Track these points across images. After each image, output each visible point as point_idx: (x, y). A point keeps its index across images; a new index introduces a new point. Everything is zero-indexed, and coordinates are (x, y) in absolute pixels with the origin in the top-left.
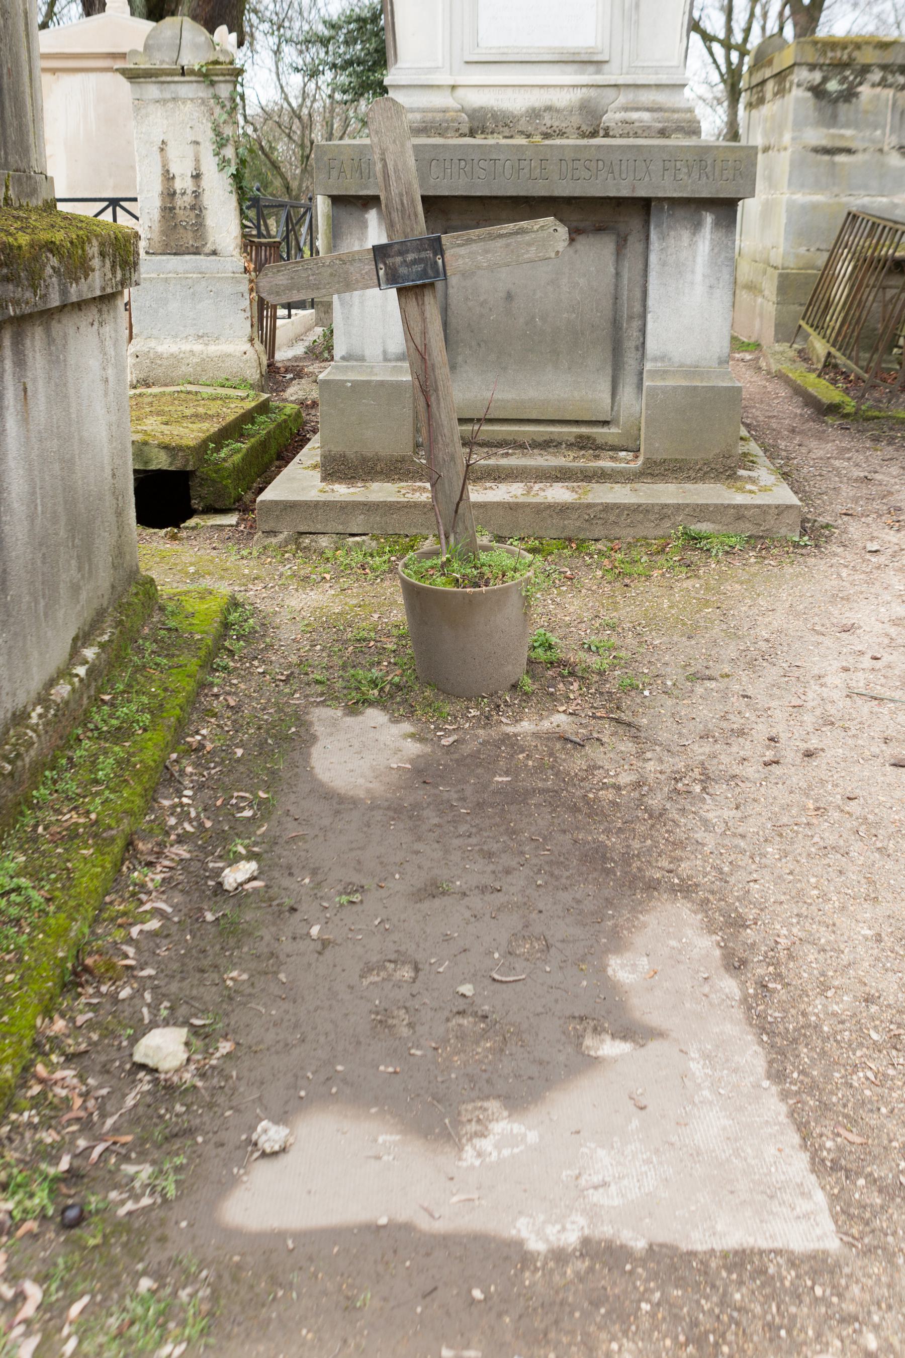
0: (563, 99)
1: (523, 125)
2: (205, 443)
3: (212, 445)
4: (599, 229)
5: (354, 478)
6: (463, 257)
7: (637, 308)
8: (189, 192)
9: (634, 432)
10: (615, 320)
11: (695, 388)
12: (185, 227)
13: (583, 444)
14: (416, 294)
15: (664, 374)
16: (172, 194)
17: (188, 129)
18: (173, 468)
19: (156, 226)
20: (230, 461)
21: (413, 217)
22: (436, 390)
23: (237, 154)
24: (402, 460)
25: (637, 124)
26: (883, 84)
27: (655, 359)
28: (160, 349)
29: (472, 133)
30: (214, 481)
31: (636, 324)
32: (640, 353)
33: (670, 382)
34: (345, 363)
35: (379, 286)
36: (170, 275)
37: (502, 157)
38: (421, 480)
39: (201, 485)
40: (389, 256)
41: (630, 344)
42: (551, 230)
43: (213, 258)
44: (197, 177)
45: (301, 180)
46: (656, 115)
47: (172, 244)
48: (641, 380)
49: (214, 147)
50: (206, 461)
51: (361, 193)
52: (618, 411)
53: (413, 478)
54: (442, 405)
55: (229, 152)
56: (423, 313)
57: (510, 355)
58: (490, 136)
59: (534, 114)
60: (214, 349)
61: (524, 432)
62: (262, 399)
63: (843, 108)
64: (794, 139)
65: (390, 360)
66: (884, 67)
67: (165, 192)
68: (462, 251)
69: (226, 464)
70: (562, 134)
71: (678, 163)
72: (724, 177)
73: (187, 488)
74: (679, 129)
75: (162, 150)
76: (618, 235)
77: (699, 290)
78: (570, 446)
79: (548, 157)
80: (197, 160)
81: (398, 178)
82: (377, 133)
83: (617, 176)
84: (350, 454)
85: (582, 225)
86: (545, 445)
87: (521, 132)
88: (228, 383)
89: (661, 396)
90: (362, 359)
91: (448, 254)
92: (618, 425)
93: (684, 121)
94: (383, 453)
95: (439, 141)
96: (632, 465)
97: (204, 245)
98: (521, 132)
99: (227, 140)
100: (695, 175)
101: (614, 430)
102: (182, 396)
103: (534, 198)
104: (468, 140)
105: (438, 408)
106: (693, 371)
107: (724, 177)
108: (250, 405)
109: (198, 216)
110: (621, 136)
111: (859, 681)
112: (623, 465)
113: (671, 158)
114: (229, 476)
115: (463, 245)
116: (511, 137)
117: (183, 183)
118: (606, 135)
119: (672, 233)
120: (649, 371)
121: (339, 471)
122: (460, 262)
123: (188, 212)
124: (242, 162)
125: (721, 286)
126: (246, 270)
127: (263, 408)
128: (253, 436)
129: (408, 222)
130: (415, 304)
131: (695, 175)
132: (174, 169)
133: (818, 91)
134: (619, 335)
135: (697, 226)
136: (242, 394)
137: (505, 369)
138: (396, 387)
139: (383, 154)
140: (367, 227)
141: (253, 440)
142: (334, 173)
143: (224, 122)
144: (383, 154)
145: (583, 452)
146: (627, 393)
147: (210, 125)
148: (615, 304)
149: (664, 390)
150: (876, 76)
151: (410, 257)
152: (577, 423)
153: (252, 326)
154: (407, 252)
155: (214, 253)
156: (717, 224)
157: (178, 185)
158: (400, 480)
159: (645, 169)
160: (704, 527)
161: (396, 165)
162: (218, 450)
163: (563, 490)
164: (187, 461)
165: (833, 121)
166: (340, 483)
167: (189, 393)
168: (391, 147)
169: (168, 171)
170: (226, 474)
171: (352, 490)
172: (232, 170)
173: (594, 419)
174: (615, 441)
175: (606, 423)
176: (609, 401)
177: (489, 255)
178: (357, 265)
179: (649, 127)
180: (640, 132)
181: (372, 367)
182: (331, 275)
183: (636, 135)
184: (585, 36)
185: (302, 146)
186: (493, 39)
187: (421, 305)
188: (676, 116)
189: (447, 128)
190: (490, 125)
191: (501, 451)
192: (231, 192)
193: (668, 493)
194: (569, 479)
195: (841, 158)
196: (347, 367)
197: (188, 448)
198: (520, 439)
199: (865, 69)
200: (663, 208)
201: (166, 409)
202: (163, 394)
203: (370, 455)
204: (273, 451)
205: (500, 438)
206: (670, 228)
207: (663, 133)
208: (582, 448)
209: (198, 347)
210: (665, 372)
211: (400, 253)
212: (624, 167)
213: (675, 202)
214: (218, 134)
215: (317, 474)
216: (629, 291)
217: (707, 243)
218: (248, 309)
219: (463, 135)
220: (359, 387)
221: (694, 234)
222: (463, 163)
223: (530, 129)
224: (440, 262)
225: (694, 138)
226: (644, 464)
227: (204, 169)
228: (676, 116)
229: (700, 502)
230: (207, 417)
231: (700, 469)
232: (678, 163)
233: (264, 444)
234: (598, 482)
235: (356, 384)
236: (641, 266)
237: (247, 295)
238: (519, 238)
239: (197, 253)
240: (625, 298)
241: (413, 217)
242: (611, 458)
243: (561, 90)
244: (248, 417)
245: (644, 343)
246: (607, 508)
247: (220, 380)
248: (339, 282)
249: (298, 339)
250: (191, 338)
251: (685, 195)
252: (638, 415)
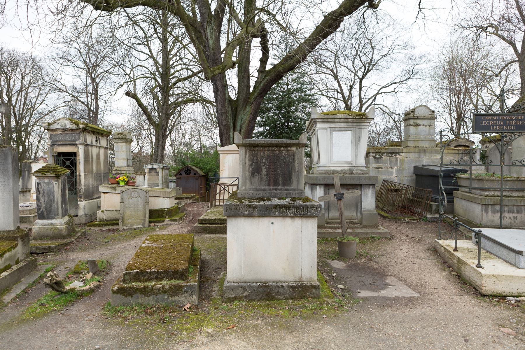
0: (346, 168)
26: (387, 156)
59: (342, 171)
63: (380, 160)
66: (387, 153)
77: (370, 198)
95: (327, 175)
106: (370, 211)
111: (405, 255)
133: (375, 157)
135: (369, 188)
150: (386, 154)
160: (374, 236)
165: (378, 163)
184: (349, 159)
186: (335, 159)
193: (367, 230)
195: (380, 169)
199: (383, 153)
207: (363, 174)
213: (366, 184)
226: (335, 268)
229: (317, 242)
243: (346, 167)
246: (358, 233)
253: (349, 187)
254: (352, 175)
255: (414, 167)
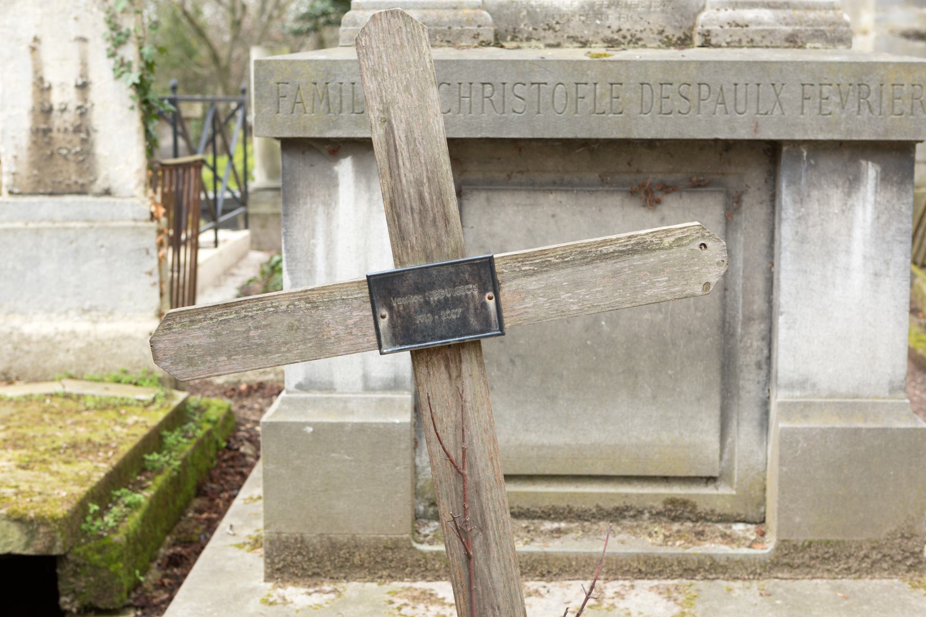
1: (575, 27)
2: (82, 506)
3: (94, 507)
4: (698, 185)
5: (318, 574)
6: (534, 294)
7: (759, 305)
8: (72, 107)
9: (756, 493)
10: (724, 321)
11: (857, 431)
12: (65, 157)
13: (676, 511)
14: (447, 360)
15: (804, 409)
16: (47, 112)
17: (71, 21)
18: (30, 552)
19: (24, 156)
20: (122, 531)
21: (440, 224)
22: (483, 528)
23: (141, 56)
24: (395, 546)
25: (753, 27)
27: (791, 386)
28: (27, 329)
29: (498, 41)
30: (96, 567)
31: (758, 328)
32: (763, 373)
33: (816, 423)
34: (303, 395)
35: (380, 347)
36: (44, 225)
37: (550, 79)
38: (424, 578)
39: (75, 574)
40: (398, 295)
41: (748, 358)
42: (696, 245)
43: (106, 199)
44: (83, 87)
45: (232, 49)
46: (781, 14)
47: (48, 180)
48: (766, 414)
49: (109, 45)
50: (85, 533)
51: (328, 135)
52: (731, 460)
53: (412, 576)
54: (494, 553)
55: (130, 52)
56: (459, 395)
57: (561, 377)
58: (524, 44)
60: (106, 329)
61: (584, 495)
62: (175, 403)
64: (877, 21)
65: (373, 390)
67: (38, 108)
68: (532, 283)
69: (116, 538)
70: (635, 41)
71: (825, 89)
72: (897, 110)
73: (54, 578)
74: (818, 35)
75: (33, 49)
76: (728, 194)
77: (858, 279)
78: (657, 516)
79: (622, 79)
80: (84, 64)
81: (414, 153)
82: (375, 73)
83: (730, 108)
84: (312, 537)
85: (670, 179)
86: (618, 514)
87: (573, 39)
88: (125, 378)
89: (803, 444)
90: (329, 387)
91: (506, 291)
92: (730, 482)
93: (825, 22)
94: (364, 536)
96: (757, 551)
97: (93, 182)
98: (573, 39)
99: (127, 36)
100: (852, 107)
101: (723, 490)
102: (57, 403)
103: (597, 140)
104: (492, 53)
105: (487, 559)
106: (850, 405)
107: (897, 110)
108: (157, 416)
109: (84, 141)
110: (729, 45)
112: (744, 551)
113: (814, 81)
114: (120, 557)
115: (533, 273)
116: (558, 45)
117: (63, 96)
118: (707, 44)
119: (815, 194)
120: (782, 405)
121: (294, 564)
122: (529, 303)
123: (70, 137)
124: (149, 66)
125: (891, 273)
126: (153, 217)
127: (178, 418)
128: (160, 471)
129: (431, 231)
130: (444, 376)
131: (852, 107)
132: (50, 77)
134: (732, 346)
135: (854, 182)
136: (144, 394)
137: (553, 399)
138: (384, 433)
139: (386, 110)
140: (336, 185)
141: (160, 479)
142: (286, 104)
143: (124, 11)
144: (386, 110)
145: (676, 526)
146: (744, 434)
147: (102, 15)
148: (724, 297)
149: (808, 435)
151: (436, 296)
152: (666, 479)
153: (161, 295)
154: (432, 286)
155: (107, 192)
156: (884, 179)
157: (56, 98)
158: (391, 577)
159: (773, 97)
161: (409, 131)
162: (100, 514)
163: (653, 596)
164: (53, 540)
166: (295, 584)
167: (67, 396)
168: (401, 99)
169: (41, 79)
170: (114, 554)
171: (316, 599)
172: (134, 77)
173: (693, 474)
174: (727, 508)
175: (710, 480)
176: (716, 446)
177: (582, 291)
178: (339, 309)
179: (771, 32)
180: (757, 38)
181: (346, 401)
182: (291, 327)
183: (752, 44)
185: (233, 10)
187: (456, 378)
188: (812, 15)
189: (460, 34)
190: (525, 27)
191: (548, 525)
192: (132, 108)
194: (660, 574)
196: (305, 400)
197: (55, 520)
198: (578, 506)
200: (800, 156)
201: (31, 433)
202: (29, 398)
203: (342, 539)
204: (190, 487)
205: (546, 504)
206: (811, 185)
207: (793, 41)
208: (675, 519)
209: (83, 326)
210: (808, 405)
211: (419, 289)
212: (741, 95)
213: (818, 147)
214: (115, 27)
215: (256, 561)
216: (746, 278)
217: (870, 208)
218: (156, 272)
219: (485, 44)
220: (328, 436)
221: (849, 194)
222: (488, 88)
223: (586, 33)
224: (491, 304)
225: (841, 48)
226: (777, 548)
227: (93, 77)
228: (812, 15)
230: (93, 447)
231: (866, 556)
232: (825, 89)
233: (176, 483)
234: (705, 578)
235: (320, 429)
236: (763, 241)
237: (154, 252)
238: (637, 260)
239: (82, 191)
240: (739, 288)
241: (440, 224)
242: (724, 536)
244: (154, 441)
245: (769, 358)
247: (114, 374)
248: (304, 341)
249: (228, 272)
250: (72, 313)
251: (837, 137)
252: (761, 468)
253: (656, 170)
254: (694, 54)
255: (265, 581)
